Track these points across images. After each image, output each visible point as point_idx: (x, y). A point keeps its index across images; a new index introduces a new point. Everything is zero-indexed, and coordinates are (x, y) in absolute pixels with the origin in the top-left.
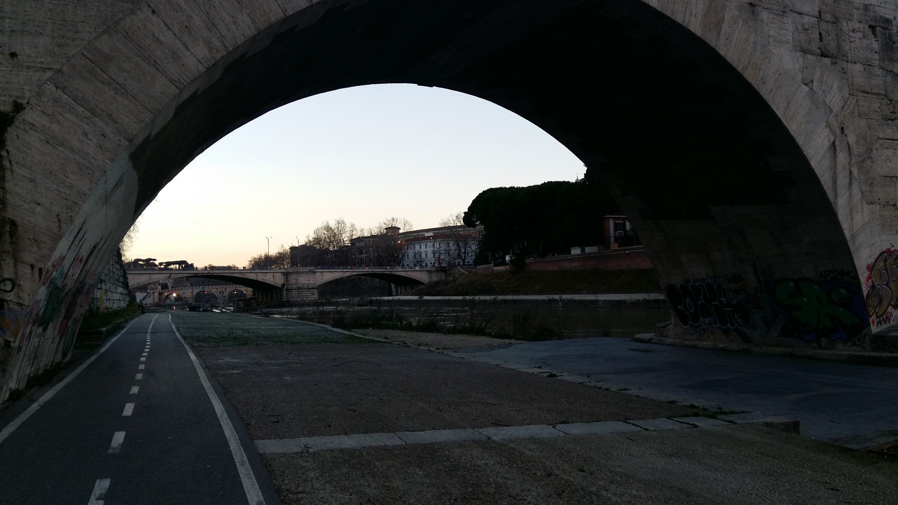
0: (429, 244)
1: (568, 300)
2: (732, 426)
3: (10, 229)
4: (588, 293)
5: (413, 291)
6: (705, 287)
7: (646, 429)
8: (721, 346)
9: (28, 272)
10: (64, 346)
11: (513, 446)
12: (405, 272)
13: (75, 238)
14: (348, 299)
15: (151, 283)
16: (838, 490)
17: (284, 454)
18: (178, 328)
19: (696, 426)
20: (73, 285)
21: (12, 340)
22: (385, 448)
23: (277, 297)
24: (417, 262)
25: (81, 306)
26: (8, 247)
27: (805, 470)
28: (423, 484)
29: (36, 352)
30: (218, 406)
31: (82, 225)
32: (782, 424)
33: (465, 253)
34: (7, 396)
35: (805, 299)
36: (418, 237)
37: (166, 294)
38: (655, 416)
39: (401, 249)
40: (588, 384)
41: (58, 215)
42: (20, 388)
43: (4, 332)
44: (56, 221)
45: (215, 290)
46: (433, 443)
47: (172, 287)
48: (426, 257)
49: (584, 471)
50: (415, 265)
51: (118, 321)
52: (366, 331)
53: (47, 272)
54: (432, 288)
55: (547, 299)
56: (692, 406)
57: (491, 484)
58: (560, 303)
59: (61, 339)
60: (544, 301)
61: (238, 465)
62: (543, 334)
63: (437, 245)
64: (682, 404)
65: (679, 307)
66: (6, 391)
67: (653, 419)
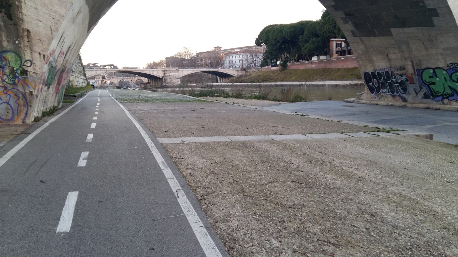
0: (237, 56)
1: (310, 84)
2: (398, 136)
3: (27, 34)
4: (320, 81)
5: (229, 80)
6: (384, 73)
7: (353, 137)
8: (391, 103)
9: (38, 56)
10: (58, 99)
11: (286, 143)
12: (224, 71)
13: (60, 40)
14: (196, 84)
15: (96, 75)
16: (454, 163)
17: (172, 144)
18: (112, 95)
19: (379, 136)
20: (60, 67)
21: (33, 91)
22: (222, 142)
23: (160, 83)
24: (231, 65)
25: (65, 79)
26: (26, 44)
27: (436, 155)
28: (242, 156)
29: (45, 100)
30: (138, 125)
31: (63, 34)
32: (424, 136)
33: (256, 61)
34: (33, 120)
35: (438, 79)
36: (231, 52)
37: (104, 81)
38: (357, 131)
39: (223, 58)
40: (322, 119)
41: (50, 27)
42: (39, 116)
43: (29, 87)
44: (50, 30)
45: (129, 79)
46: (245, 141)
47: (107, 78)
48: (236, 63)
49: (322, 153)
50: (230, 67)
51: (83, 91)
52: (206, 98)
53: (48, 57)
54: (239, 79)
55: (298, 84)
56: (377, 128)
57: (275, 157)
58: (305, 86)
59: (56, 94)
60: (297, 85)
61: (150, 147)
62: (297, 99)
63: (241, 56)
64: (371, 127)
65: (370, 84)
66: (32, 117)
67: (357, 132)
